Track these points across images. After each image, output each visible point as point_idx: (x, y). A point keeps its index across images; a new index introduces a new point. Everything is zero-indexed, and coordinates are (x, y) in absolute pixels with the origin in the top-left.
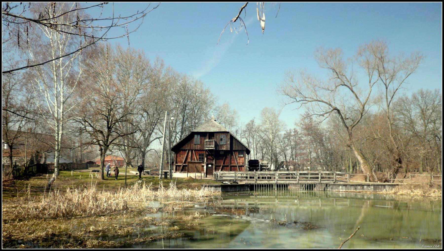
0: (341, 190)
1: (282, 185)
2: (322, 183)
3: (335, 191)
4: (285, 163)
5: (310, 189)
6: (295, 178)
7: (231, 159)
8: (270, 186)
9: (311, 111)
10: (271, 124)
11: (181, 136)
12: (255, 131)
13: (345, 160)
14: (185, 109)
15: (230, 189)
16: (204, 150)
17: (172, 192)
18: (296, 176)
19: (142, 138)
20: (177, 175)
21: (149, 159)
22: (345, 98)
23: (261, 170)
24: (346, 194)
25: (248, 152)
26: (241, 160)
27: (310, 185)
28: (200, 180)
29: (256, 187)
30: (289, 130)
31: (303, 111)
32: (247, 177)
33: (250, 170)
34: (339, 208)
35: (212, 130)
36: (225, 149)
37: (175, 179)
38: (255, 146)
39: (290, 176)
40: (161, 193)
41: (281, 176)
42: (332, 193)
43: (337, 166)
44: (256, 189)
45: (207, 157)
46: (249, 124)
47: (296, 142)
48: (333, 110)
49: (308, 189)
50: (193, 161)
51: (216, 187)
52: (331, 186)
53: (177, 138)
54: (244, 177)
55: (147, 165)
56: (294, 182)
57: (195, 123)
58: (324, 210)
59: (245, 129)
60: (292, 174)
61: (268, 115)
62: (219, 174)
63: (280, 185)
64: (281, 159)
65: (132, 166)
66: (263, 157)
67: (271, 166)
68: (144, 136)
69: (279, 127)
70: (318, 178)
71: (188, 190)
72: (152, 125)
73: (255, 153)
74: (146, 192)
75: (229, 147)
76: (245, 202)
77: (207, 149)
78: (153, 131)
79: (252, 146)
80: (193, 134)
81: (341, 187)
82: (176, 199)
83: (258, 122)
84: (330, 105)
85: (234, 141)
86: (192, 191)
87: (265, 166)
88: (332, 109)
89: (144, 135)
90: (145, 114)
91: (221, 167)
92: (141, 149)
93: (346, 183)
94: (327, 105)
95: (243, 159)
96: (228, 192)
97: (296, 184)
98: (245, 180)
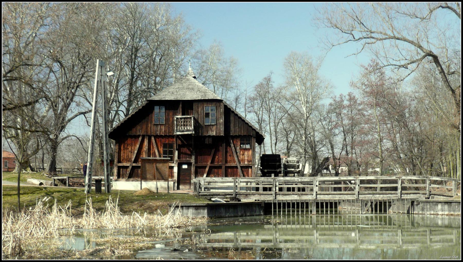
0: (440, 213)
1: (327, 204)
2: (403, 200)
3: (428, 214)
4: (331, 160)
5: (381, 211)
7: (226, 152)
8: (304, 205)
9: (381, 59)
10: (304, 84)
11: (128, 110)
12: (273, 98)
14: (136, 56)
15: (224, 212)
16: (173, 136)
17: (112, 219)
18: (352, 186)
19: (51, 113)
20: (122, 185)
21: (66, 155)
23: (286, 174)
25: (260, 139)
26: (247, 155)
27: (381, 203)
28: (165, 195)
29: (275, 208)
30: (338, 96)
31: (366, 59)
32: (257, 189)
35: (189, 96)
36: (214, 134)
37: (116, 193)
38: (272, 128)
39: (342, 186)
40: (89, 221)
41: (323, 186)
42: (423, 219)
43: (432, 165)
44: (275, 211)
45: (179, 150)
46: (261, 86)
47: (352, 119)
48: (424, 57)
49: (376, 211)
50: (151, 158)
52: (421, 205)
53: (120, 113)
55: (63, 166)
57: (155, 83)
59: (252, 95)
60: (345, 182)
61: (297, 66)
62: (202, 183)
63: (322, 204)
64: (324, 152)
65: (32, 170)
66: (289, 149)
67: (304, 167)
68: (54, 110)
69: (320, 91)
70: (395, 189)
71: (142, 215)
72: (71, 88)
73: (274, 142)
74: (58, 219)
75: (222, 129)
77: (179, 133)
78: (72, 100)
80: (151, 105)
81: (440, 206)
82: (119, 232)
83: (278, 82)
84: (420, 47)
85: (232, 118)
86: (151, 217)
87: (293, 167)
88: (423, 54)
89: (54, 106)
90: (56, 67)
91: (207, 169)
92: (49, 135)
93: (450, 199)
94: (413, 47)
95: (250, 152)
96: (221, 217)
97: (353, 201)
98: (253, 194)
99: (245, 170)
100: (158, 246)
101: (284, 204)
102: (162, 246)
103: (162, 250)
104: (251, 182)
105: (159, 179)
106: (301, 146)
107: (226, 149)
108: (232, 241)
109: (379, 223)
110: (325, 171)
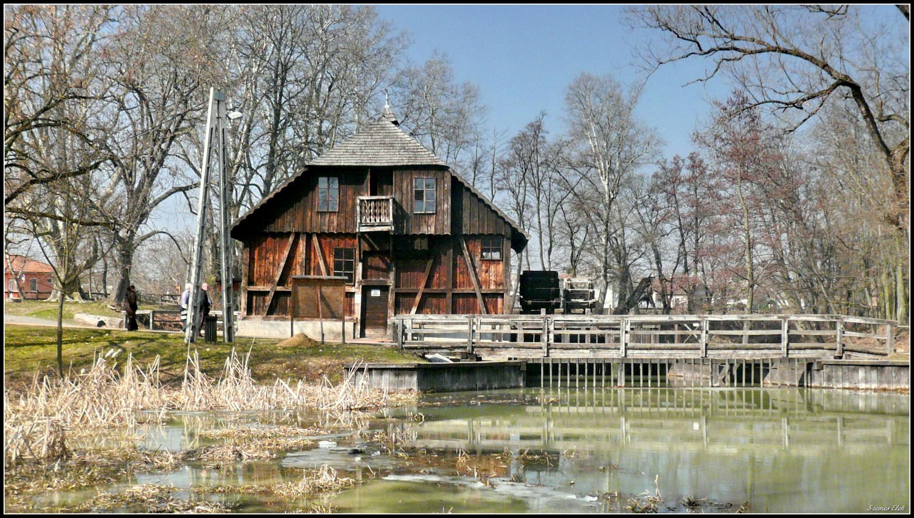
1: (645, 366)
2: (791, 360)
3: (839, 386)
4: (656, 283)
5: (748, 380)
6: (693, 339)
7: (455, 266)
9: (752, 89)
10: (606, 137)
11: (267, 184)
12: (546, 163)
13: (878, 273)
14: (284, 79)
15: (449, 380)
16: (353, 236)
17: (237, 392)
19: (121, 187)
20: (253, 328)
22: (881, 43)
24: (880, 397)
25: (519, 242)
26: (495, 271)
27: (748, 365)
30: (670, 159)
31: (723, 89)
32: (513, 338)
33: (527, 309)
34: (856, 450)
35: (385, 159)
36: (432, 231)
37: (246, 343)
38: (544, 221)
39: (676, 332)
40: (193, 394)
42: (829, 397)
43: (849, 294)
44: (547, 381)
45: (363, 261)
46: (522, 138)
48: (834, 87)
49: (740, 381)
51: (398, 371)
52: (826, 370)
54: (505, 336)
56: (691, 355)
57: (320, 133)
58: (800, 460)
59: (506, 157)
60: (681, 325)
61: (593, 102)
62: (408, 324)
63: (637, 366)
65: (84, 296)
66: (574, 261)
68: (127, 183)
69: (637, 150)
70: (777, 339)
71: (293, 384)
72: (159, 140)
73: (546, 247)
74: (135, 391)
75: (448, 222)
76: (508, 430)
77: (364, 229)
78: (161, 163)
79: (536, 219)
81: (861, 373)
83: (556, 131)
84: (825, 66)
85: (466, 201)
86: (310, 389)
87: (583, 295)
88: (832, 81)
89: (127, 176)
90: (132, 99)
91: (418, 299)
92: (118, 234)
94: (814, 69)
95: (501, 267)
96: (443, 391)
97: (696, 362)
98: (506, 347)
99: (491, 299)
100: (323, 444)
101: (564, 366)
102: (332, 445)
103: (332, 452)
104: (501, 324)
105: (325, 317)
106: (599, 256)
107: (455, 260)
108: (464, 437)
109: (744, 403)
110: (644, 304)
